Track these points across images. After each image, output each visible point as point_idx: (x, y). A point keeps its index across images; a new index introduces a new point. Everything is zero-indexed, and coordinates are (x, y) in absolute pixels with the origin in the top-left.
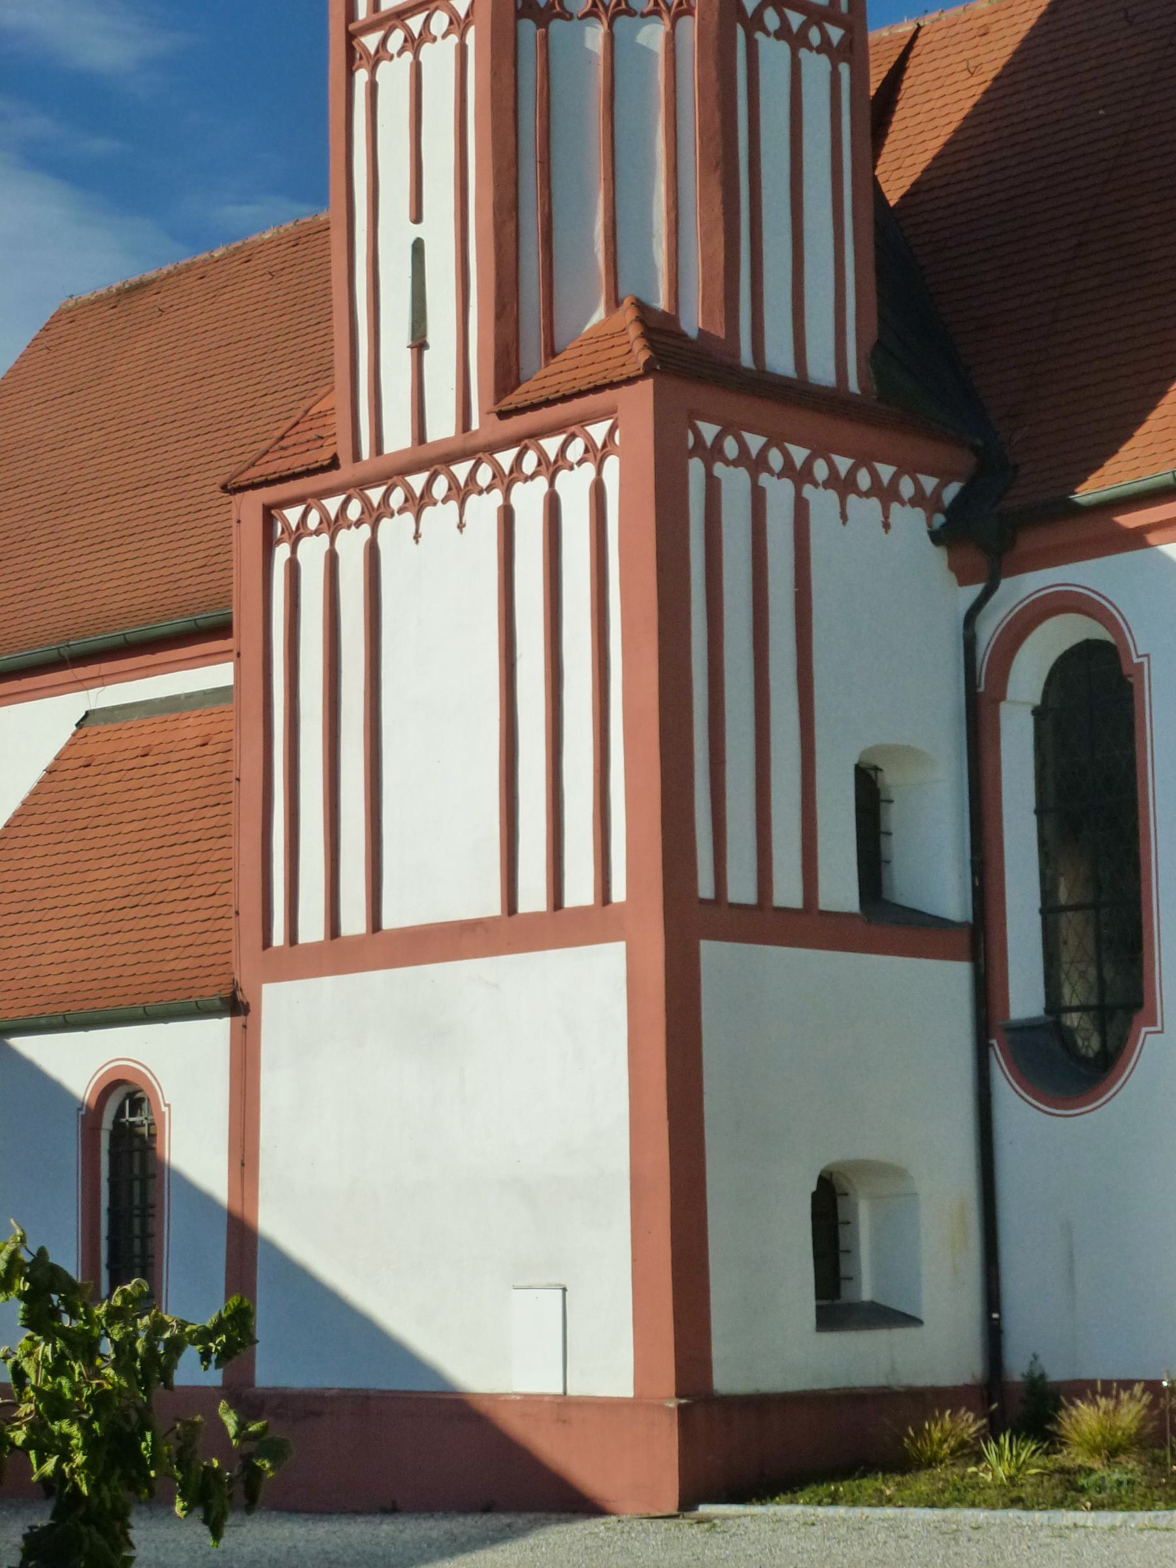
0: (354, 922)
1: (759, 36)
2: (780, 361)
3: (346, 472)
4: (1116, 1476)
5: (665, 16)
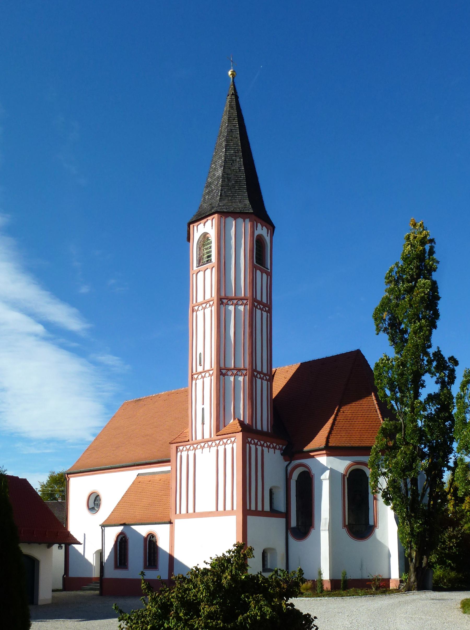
0: (191, 510)
1: (257, 378)
2: (259, 428)
3: (190, 442)
4: (308, 593)
5: (243, 376)
